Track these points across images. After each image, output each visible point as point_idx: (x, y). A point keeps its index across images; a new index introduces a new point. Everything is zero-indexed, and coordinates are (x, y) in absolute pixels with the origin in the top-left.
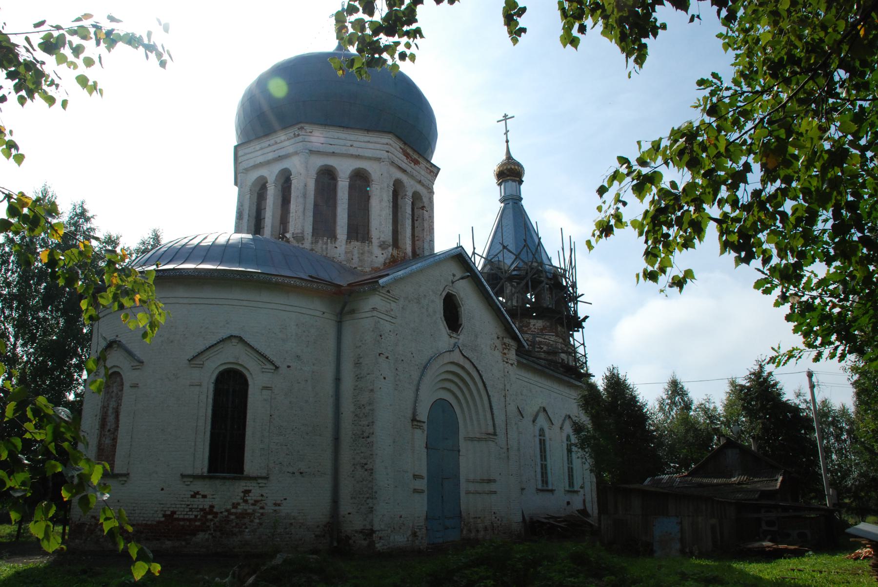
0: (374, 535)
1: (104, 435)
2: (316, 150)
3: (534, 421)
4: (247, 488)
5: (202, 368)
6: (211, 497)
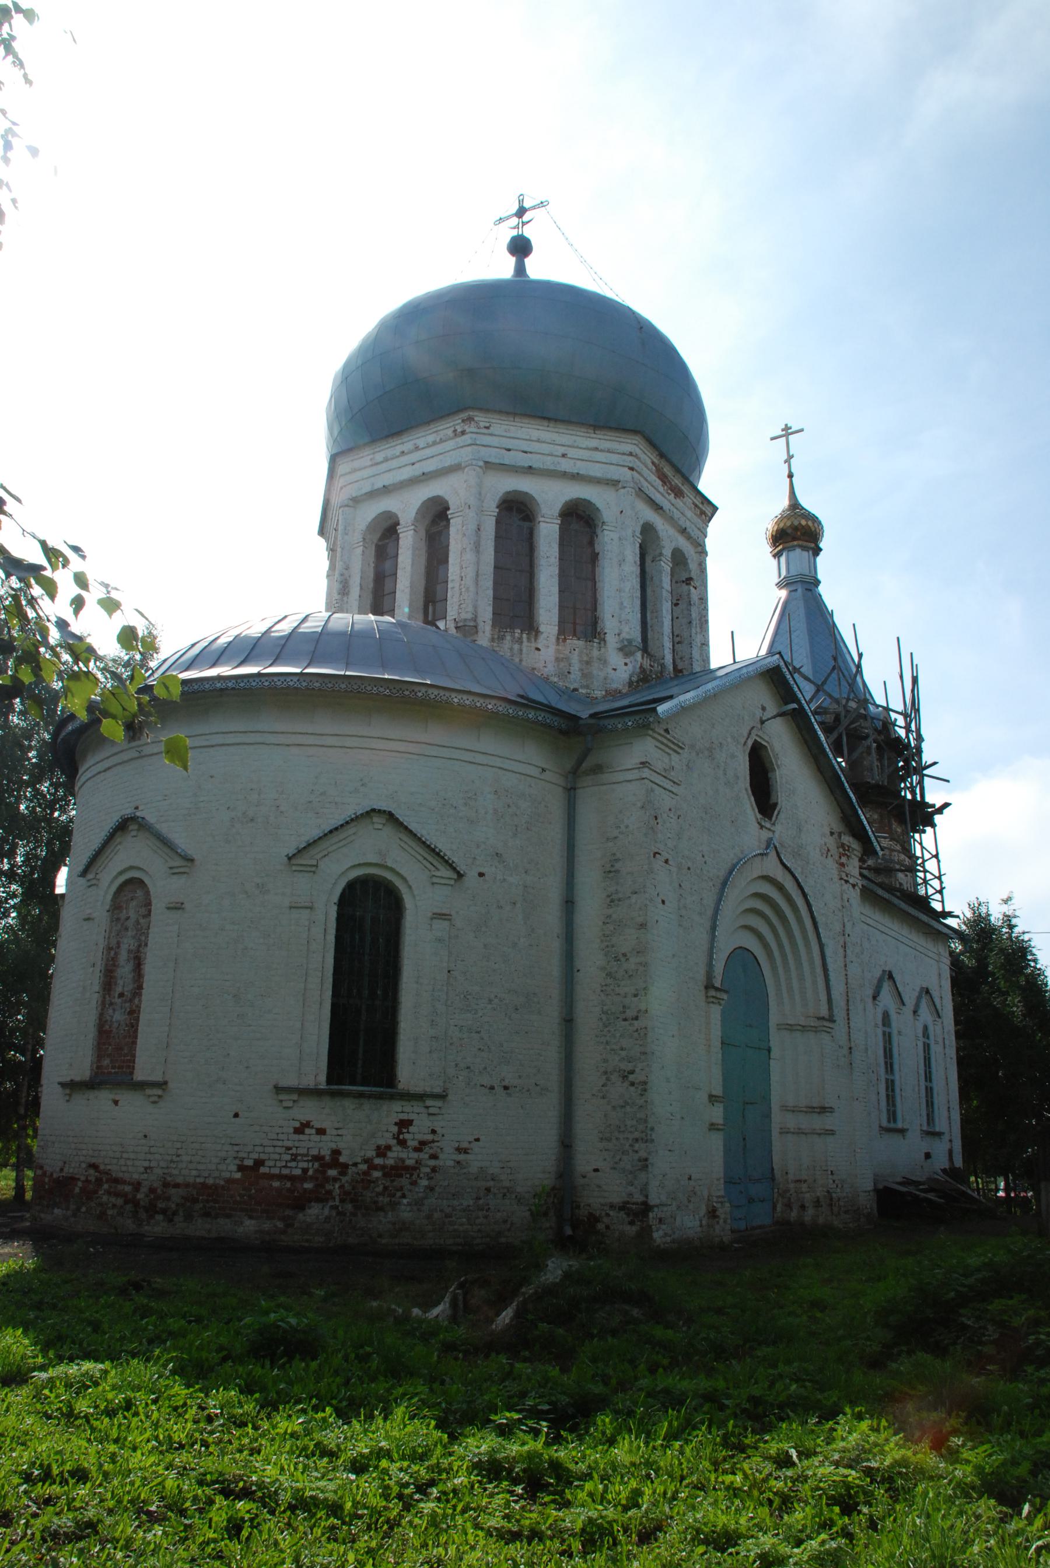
0: (651, 1215)
1: (111, 1004)
2: (497, 461)
3: (874, 998)
4: (405, 1117)
5: (314, 872)
6: (335, 1132)
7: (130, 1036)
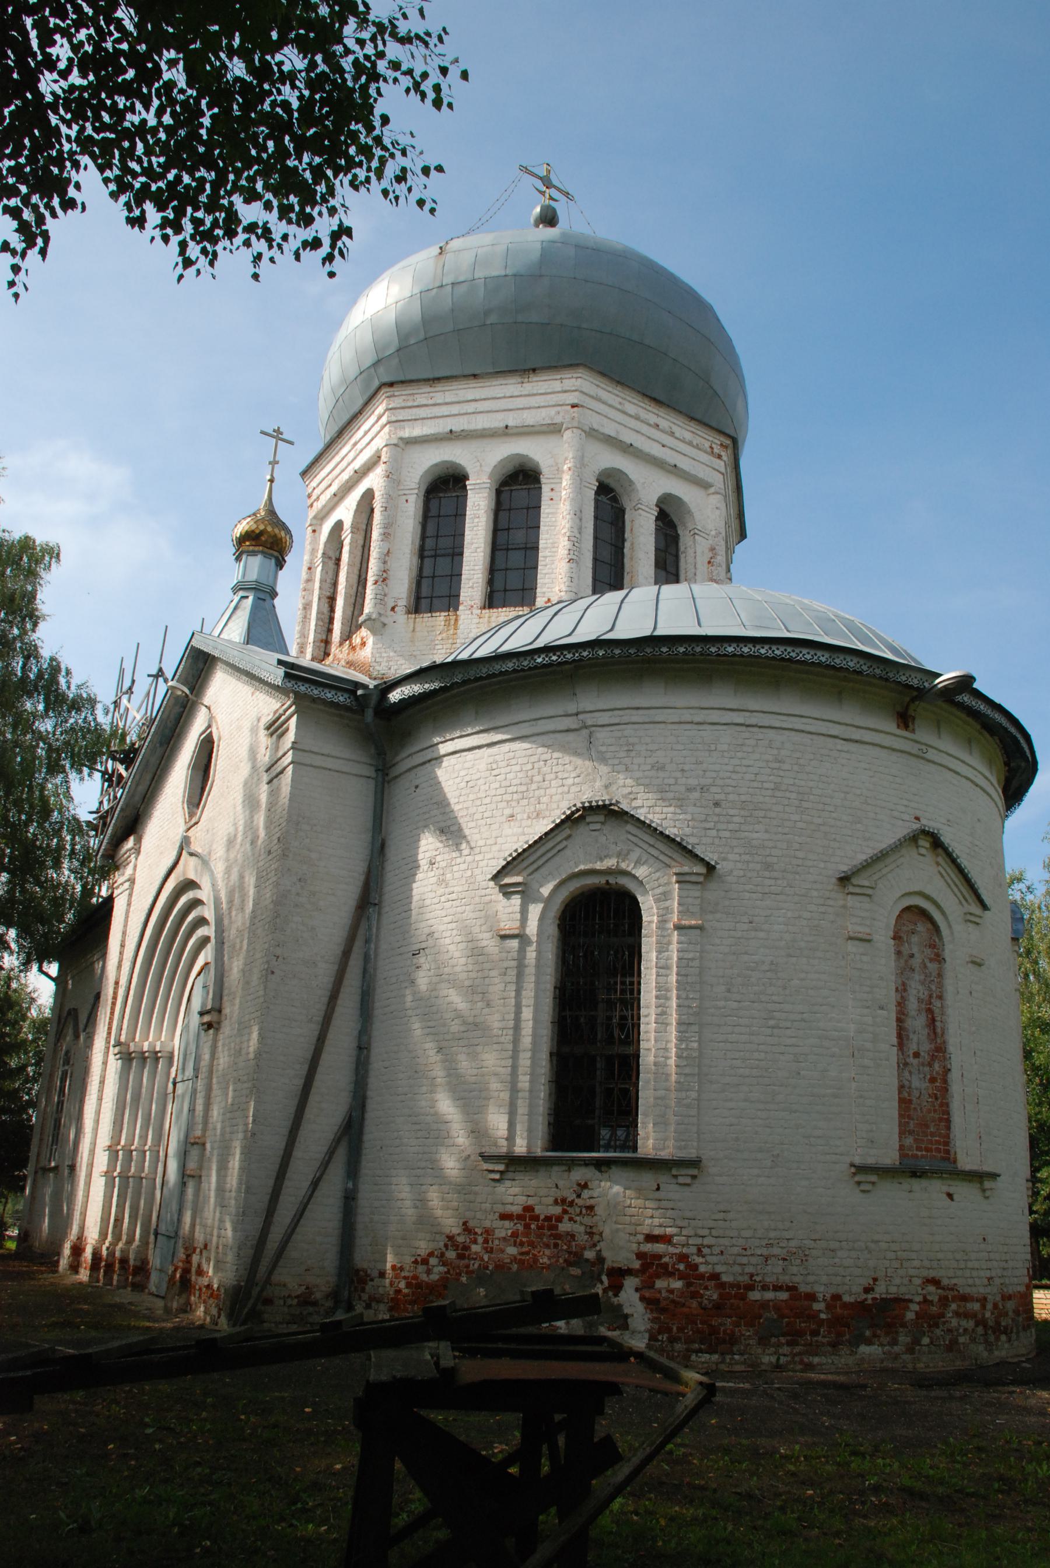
7: (935, 1111)
